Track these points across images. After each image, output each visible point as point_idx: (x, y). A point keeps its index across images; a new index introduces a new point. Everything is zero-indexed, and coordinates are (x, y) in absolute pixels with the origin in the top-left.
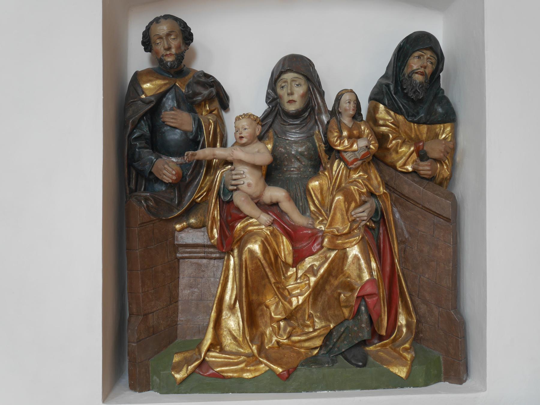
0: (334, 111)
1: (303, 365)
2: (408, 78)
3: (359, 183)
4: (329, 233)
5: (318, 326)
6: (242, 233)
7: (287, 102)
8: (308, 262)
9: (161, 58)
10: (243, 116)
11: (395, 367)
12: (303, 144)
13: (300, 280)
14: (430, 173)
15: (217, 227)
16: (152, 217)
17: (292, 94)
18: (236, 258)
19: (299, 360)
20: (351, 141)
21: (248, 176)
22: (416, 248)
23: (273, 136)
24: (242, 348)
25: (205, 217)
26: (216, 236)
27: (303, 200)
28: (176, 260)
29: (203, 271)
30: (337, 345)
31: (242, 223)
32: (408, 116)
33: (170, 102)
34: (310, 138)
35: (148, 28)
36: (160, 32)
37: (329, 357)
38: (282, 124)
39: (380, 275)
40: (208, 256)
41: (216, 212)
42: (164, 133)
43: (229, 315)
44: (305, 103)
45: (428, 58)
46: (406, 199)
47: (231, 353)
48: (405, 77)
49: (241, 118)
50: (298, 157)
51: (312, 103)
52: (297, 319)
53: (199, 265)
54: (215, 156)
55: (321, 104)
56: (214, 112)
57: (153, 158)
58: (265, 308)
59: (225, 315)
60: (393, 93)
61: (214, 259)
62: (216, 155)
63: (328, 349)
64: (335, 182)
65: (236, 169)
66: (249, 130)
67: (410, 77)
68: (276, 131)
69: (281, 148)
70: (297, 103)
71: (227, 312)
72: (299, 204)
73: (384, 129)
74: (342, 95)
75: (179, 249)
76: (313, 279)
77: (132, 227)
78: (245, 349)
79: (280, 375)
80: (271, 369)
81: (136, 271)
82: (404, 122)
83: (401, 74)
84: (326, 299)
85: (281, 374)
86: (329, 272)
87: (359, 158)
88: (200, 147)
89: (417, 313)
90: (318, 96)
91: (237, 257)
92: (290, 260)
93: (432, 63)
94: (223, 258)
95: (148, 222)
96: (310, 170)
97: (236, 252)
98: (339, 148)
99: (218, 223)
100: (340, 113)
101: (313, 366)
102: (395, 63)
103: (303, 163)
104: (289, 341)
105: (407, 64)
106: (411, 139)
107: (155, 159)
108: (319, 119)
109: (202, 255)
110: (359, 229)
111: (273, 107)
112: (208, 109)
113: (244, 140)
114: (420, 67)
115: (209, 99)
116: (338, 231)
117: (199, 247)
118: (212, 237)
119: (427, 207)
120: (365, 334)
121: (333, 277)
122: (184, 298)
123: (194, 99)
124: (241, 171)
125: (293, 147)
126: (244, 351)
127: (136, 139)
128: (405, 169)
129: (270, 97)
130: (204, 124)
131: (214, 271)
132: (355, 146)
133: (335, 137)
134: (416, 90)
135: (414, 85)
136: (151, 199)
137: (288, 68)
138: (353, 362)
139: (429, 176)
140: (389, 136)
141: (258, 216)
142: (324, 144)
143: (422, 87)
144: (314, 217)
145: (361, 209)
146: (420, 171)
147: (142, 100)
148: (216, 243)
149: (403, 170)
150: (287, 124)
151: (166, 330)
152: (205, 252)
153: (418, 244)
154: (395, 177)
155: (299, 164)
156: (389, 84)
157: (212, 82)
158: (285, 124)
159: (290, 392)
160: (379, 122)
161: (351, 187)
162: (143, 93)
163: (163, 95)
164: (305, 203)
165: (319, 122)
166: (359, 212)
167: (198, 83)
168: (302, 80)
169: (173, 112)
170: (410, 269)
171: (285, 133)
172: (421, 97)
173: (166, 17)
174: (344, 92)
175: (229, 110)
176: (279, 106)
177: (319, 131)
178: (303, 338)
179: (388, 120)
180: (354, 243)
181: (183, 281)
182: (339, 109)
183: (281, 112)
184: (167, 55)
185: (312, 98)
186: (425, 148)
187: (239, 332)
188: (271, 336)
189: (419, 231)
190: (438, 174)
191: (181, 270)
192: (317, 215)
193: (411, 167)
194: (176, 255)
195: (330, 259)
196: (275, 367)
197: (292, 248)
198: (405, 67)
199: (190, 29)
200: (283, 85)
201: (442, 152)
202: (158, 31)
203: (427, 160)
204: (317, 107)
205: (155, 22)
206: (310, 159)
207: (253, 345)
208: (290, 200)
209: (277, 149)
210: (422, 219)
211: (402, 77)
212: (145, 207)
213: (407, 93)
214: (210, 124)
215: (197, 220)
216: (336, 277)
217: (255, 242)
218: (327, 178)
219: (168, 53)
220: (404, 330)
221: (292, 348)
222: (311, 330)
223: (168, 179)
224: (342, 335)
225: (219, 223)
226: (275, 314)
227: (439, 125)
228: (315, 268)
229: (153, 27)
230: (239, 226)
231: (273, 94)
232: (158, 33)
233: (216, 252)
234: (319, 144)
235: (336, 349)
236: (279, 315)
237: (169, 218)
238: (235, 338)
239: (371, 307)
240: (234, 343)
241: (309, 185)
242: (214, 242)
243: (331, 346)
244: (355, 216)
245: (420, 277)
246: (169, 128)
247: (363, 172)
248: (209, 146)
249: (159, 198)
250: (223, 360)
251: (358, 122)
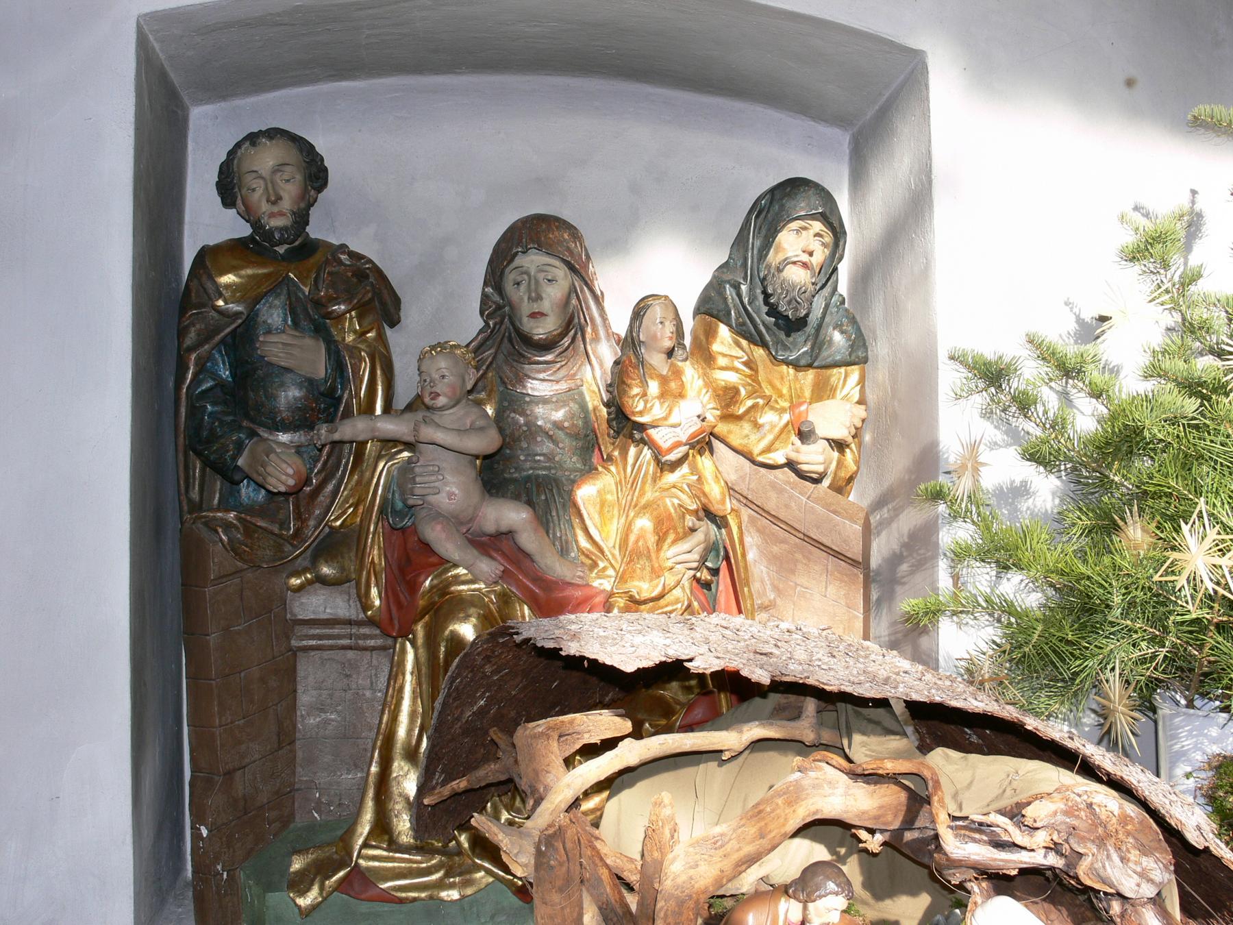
16: (239, 564)
18: (421, 651)
41: (376, 552)
43: (406, 768)
45: (817, 235)
51: (579, 318)
55: (598, 320)
59: (397, 770)
61: (372, 651)
69: (514, 412)
71: (403, 764)
72: (554, 534)
77: (197, 586)
87: (684, 441)
95: (230, 575)
97: (420, 629)
111: (495, 325)
117: (338, 624)
118: (365, 605)
119: (814, 537)
122: (309, 733)
152: (351, 635)
173: (274, 133)
181: (305, 698)
186: (810, 418)
189: (797, 584)
199: (322, 160)
200: (519, 279)
209: (506, 415)
210: (804, 561)
217: (466, 618)
219: (275, 209)
231: (497, 298)
232: (255, 169)
248: (360, 413)
251: (680, 364)
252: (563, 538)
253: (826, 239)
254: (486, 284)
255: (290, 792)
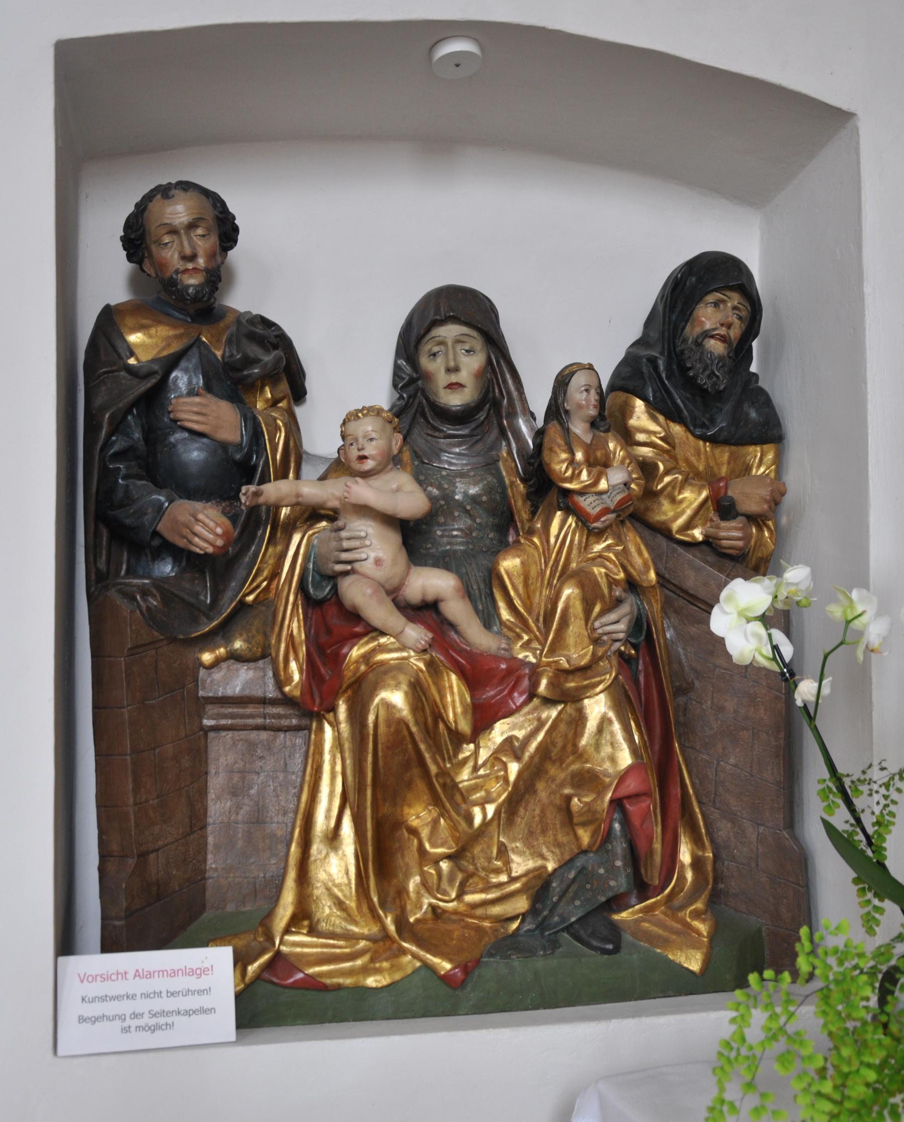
0: (554, 408)
1: (491, 955)
2: (694, 347)
3: (608, 560)
4: (551, 667)
5: (517, 870)
6: (363, 668)
7: (445, 388)
8: (500, 732)
9: (172, 277)
10: (365, 412)
11: (679, 951)
12: (479, 478)
13: (485, 771)
14: (740, 543)
15: (301, 656)
16: (156, 633)
17: (457, 370)
19: (483, 943)
20: (595, 470)
21: (375, 542)
22: (709, 702)
23: (413, 461)
24: (356, 923)
25: (266, 636)
26: (296, 677)
27: (484, 599)
28: (201, 733)
29: (262, 758)
30: (559, 910)
31: (363, 645)
32: (695, 427)
33: (181, 378)
34: (491, 465)
35: (141, 208)
36: (174, 218)
37: (543, 936)
38: (431, 436)
39: (649, 757)
40: (273, 723)
41: (295, 625)
42: (174, 446)
43: (324, 852)
44: (481, 392)
46: (689, 599)
47: (332, 935)
48: (687, 344)
49: (360, 415)
50: (468, 507)
51: (494, 391)
52: (473, 858)
53: (252, 746)
54: (300, 499)
55: (515, 394)
56: (280, 405)
57: (162, 499)
58: (406, 834)
60: (664, 375)
61: (286, 731)
62: (302, 496)
63: (540, 919)
64: (557, 561)
65: (347, 528)
66: (380, 441)
67: (698, 344)
68: (416, 449)
69: (432, 486)
70: (465, 389)
73: (646, 451)
74: (572, 374)
75: (207, 710)
76: (514, 768)
77: (110, 657)
78: (362, 927)
79: (446, 979)
80: (427, 966)
81: (120, 757)
82: (684, 439)
83: (680, 337)
84: (537, 812)
85: (450, 975)
86: (544, 751)
87: (612, 508)
88: (257, 480)
89: (712, 841)
90: (508, 376)
91: (346, 722)
92: (465, 726)
93: (740, 318)
94: (308, 728)
96: (491, 535)
98: (568, 485)
99: (302, 647)
100: (567, 412)
101: (513, 954)
102: (667, 315)
103: (478, 520)
104: (461, 905)
105: (691, 318)
106: (698, 475)
107: (166, 501)
108: (509, 427)
109: (259, 721)
110: (607, 659)
111: (409, 397)
112: (269, 396)
113: (369, 464)
114: (718, 325)
115: (270, 378)
116: (568, 661)
117: (251, 703)
120: (620, 883)
121: (554, 762)
123: (245, 373)
124: (360, 531)
125: (458, 484)
126: (361, 931)
127: (119, 456)
128: (688, 536)
129: (404, 376)
130: (267, 430)
131: (285, 758)
132: (603, 485)
133: (563, 461)
134: (713, 373)
135: (709, 362)
136: (154, 591)
137: (451, 314)
138: (595, 943)
139: (738, 552)
140: (656, 467)
141: (399, 629)
142: (521, 480)
143: (722, 367)
144: (511, 634)
145: (613, 616)
146: (721, 539)
147: (129, 369)
148: (297, 693)
149: (686, 539)
150: (442, 435)
151: (184, 890)
153: (715, 695)
154: (667, 554)
155: (469, 522)
156: (656, 358)
157: (276, 336)
158: (437, 434)
159: (467, 1014)
160: (634, 438)
161: (593, 570)
162: (132, 354)
163: (172, 362)
164: (489, 605)
165: (511, 432)
166: (610, 622)
167: (252, 337)
168: (477, 342)
169: (197, 399)
170: (698, 748)
171: (437, 453)
172: (722, 387)
173: (185, 186)
174: (575, 368)
175: (305, 401)
176: (421, 397)
177: (510, 452)
178: (490, 896)
179: (654, 433)
180: (601, 687)
181: (216, 782)
182: (566, 405)
183: (426, 409)
184: (186, 271)
185: (494, 380)
186: (730, 493)
187: (348, 888)
188: (419, 895)
189: (716, 666)
190: (751, 551)
191: (212, 755)
192: (518, 630)
193: (702, 533)
194: (201, 722)
195: (550, 723)
196: (436, 960)
197: (471, 699)
198: (686, 323)
199: (234, 218)
200: (436, 349)
201: (766, 501)
202: (167, 216)
203: (734, 518)
204: (506, 400)
205: (159, 196)
206: (492, 512)
207: (388, 914)
208: (463, 597)
211: (681, 345)
212: (144, 610)
213: (694, 378)
214: (278, 428)
215: (249, 643)
216: (561, 760)
218: (538, 551)
219: (190, 266)
220: (689, 875)
221: (463, 920)
222: (504, 878)
223: (205, 545)
224: (569, 887)
225: (304, 648)
226: (433, 845)
227: (753, 447)
228: (516, 744)
229: (156, 205)
230: (356, 652)
231: (408, 369)
232: (168, 221)
233: (290, 715)
234: (509, 479)
235: (556, 919)
236: (442, 846)
237: (193, 636)
238: (340, 904)
239: (636, 821)
240: (338, 913)
241: (499, 564)
242: (291, 691)
243: (545, 913)
244: (600, 631)
245: (718, 764)
246: (186, 435)
247: (614, 539)
249: (172, 590)
250: (319, 950)
251: (602, 434)
252: (485, 611)
253: (744, 313)
254: (398, 354)
255: (201, 880)
